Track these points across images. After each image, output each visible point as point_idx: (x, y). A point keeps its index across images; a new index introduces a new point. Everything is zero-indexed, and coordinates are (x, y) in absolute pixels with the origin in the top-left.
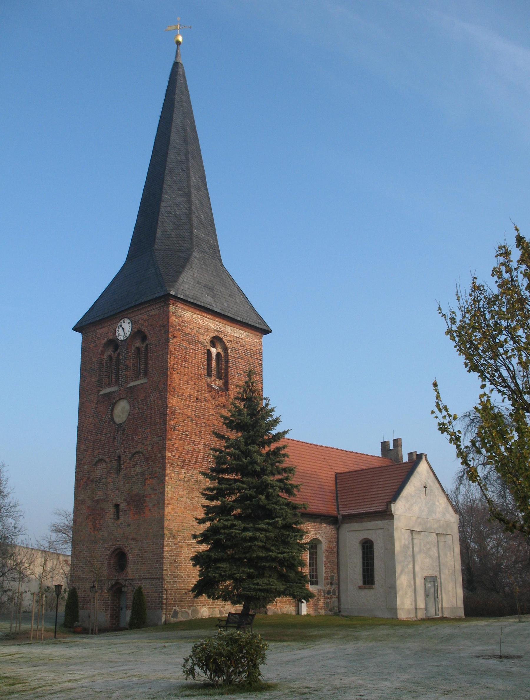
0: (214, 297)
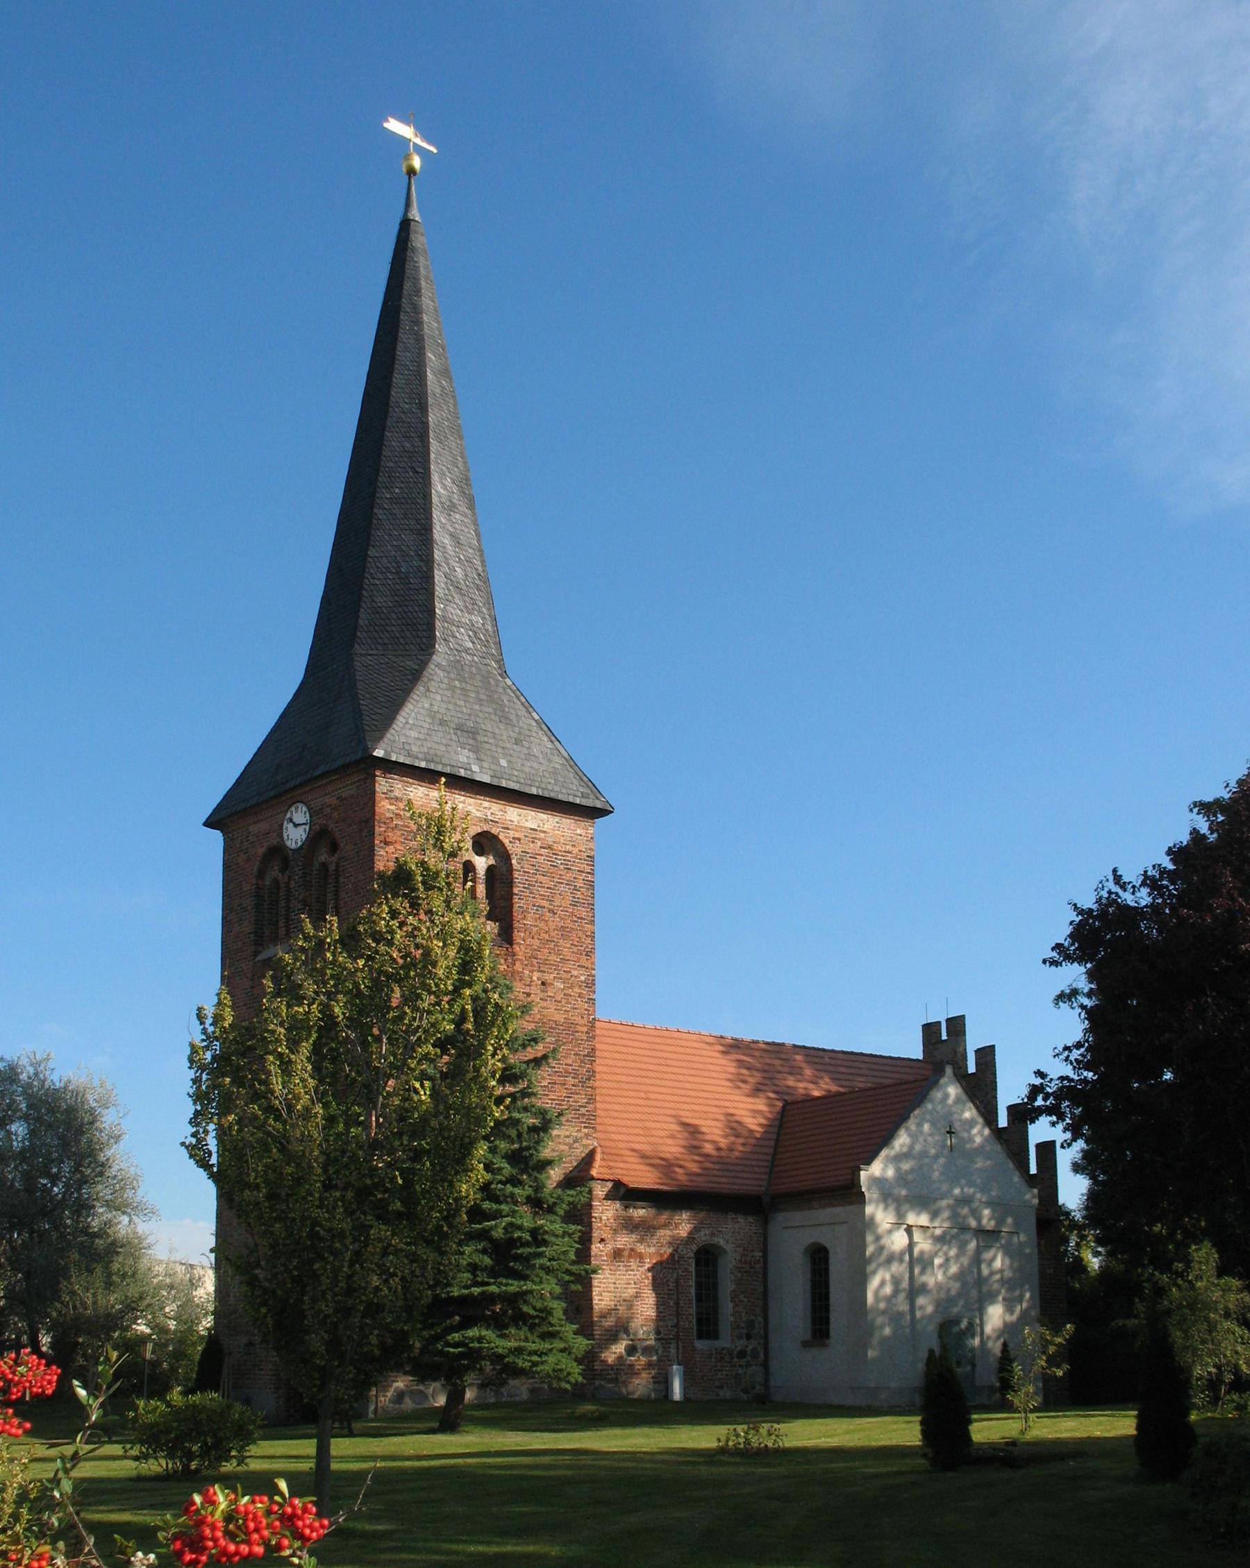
0: (476, 750)
